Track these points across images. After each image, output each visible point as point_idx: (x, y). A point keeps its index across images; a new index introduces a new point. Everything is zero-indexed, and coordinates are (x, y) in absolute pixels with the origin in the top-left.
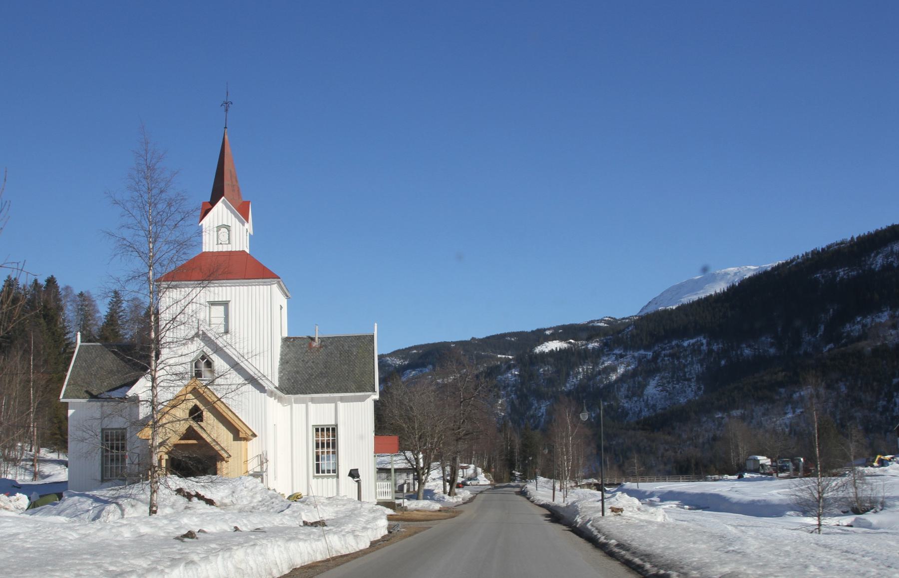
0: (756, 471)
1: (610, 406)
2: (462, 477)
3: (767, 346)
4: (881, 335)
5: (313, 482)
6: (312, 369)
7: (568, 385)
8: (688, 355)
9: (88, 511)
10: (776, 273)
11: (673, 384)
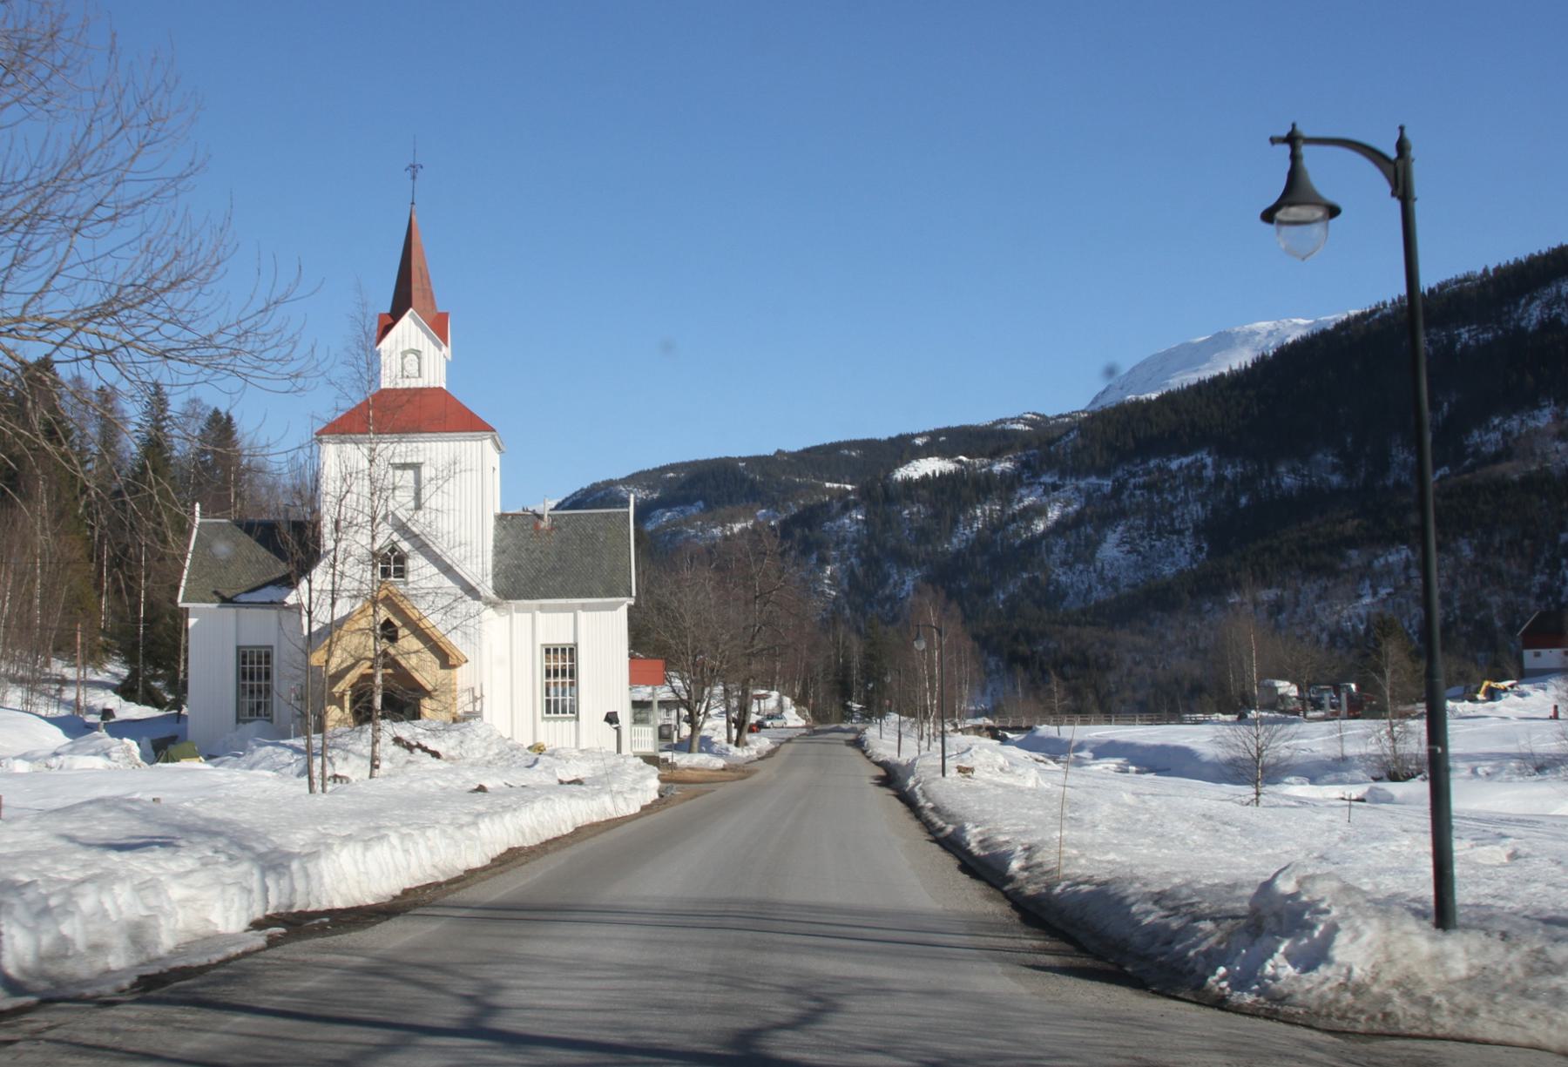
0: (1271, 707)
1: (1034, 580)
2: (758, 714)
3: (1326, 469)
4: (1538, 451)
5: (542, 725)
6: (541, 562)
7: (955, 541)
8: (1179, 487)
9: (290, 764)
10: (1343, 333)
11: (1151, 539)
